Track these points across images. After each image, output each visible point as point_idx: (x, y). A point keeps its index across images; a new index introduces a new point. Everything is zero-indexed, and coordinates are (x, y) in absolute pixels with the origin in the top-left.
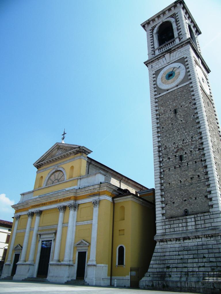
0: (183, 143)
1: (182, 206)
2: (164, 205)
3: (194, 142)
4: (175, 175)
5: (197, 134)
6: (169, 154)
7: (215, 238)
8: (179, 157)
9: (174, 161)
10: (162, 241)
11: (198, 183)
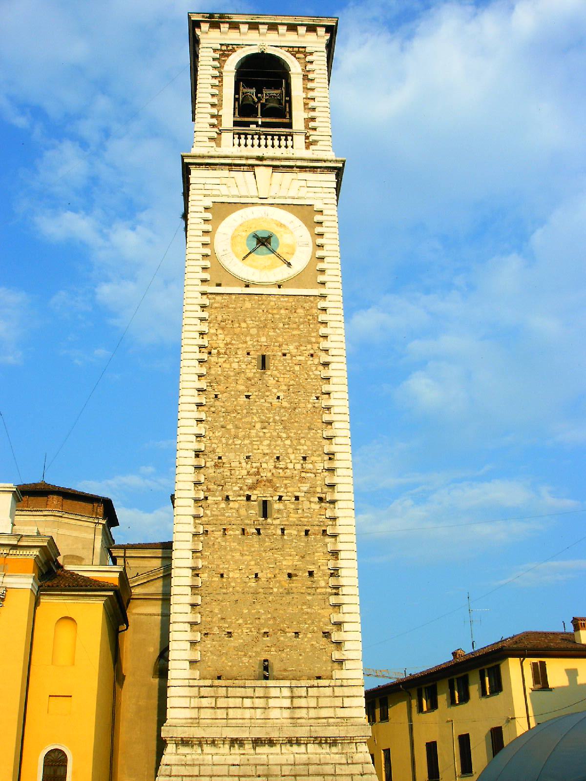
0: (275, 467)
1: (254, 649)
2: (198, 637)
3: (308, 475)
4: (242, 555)
5: (320, 455)
6: (227, 487)
7: (342, 749)
8: (259, 504)
9: (243, 512)
10: (185, 742)
11: (309, 594)
